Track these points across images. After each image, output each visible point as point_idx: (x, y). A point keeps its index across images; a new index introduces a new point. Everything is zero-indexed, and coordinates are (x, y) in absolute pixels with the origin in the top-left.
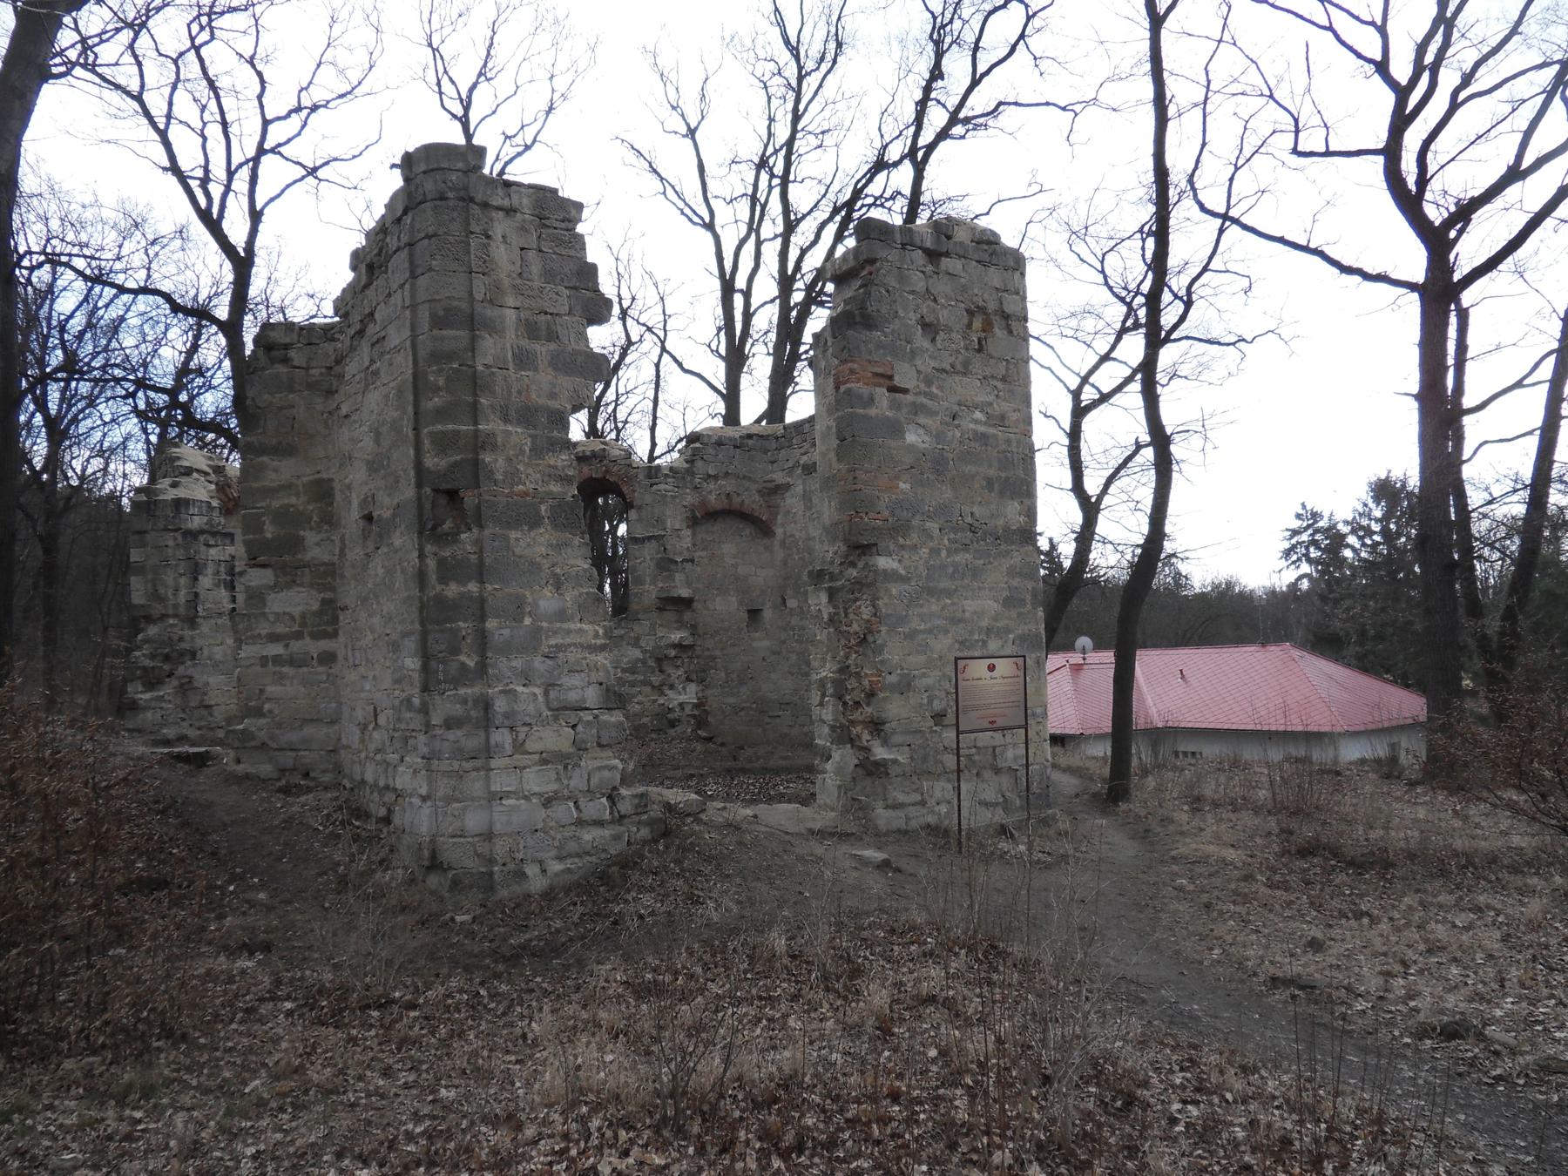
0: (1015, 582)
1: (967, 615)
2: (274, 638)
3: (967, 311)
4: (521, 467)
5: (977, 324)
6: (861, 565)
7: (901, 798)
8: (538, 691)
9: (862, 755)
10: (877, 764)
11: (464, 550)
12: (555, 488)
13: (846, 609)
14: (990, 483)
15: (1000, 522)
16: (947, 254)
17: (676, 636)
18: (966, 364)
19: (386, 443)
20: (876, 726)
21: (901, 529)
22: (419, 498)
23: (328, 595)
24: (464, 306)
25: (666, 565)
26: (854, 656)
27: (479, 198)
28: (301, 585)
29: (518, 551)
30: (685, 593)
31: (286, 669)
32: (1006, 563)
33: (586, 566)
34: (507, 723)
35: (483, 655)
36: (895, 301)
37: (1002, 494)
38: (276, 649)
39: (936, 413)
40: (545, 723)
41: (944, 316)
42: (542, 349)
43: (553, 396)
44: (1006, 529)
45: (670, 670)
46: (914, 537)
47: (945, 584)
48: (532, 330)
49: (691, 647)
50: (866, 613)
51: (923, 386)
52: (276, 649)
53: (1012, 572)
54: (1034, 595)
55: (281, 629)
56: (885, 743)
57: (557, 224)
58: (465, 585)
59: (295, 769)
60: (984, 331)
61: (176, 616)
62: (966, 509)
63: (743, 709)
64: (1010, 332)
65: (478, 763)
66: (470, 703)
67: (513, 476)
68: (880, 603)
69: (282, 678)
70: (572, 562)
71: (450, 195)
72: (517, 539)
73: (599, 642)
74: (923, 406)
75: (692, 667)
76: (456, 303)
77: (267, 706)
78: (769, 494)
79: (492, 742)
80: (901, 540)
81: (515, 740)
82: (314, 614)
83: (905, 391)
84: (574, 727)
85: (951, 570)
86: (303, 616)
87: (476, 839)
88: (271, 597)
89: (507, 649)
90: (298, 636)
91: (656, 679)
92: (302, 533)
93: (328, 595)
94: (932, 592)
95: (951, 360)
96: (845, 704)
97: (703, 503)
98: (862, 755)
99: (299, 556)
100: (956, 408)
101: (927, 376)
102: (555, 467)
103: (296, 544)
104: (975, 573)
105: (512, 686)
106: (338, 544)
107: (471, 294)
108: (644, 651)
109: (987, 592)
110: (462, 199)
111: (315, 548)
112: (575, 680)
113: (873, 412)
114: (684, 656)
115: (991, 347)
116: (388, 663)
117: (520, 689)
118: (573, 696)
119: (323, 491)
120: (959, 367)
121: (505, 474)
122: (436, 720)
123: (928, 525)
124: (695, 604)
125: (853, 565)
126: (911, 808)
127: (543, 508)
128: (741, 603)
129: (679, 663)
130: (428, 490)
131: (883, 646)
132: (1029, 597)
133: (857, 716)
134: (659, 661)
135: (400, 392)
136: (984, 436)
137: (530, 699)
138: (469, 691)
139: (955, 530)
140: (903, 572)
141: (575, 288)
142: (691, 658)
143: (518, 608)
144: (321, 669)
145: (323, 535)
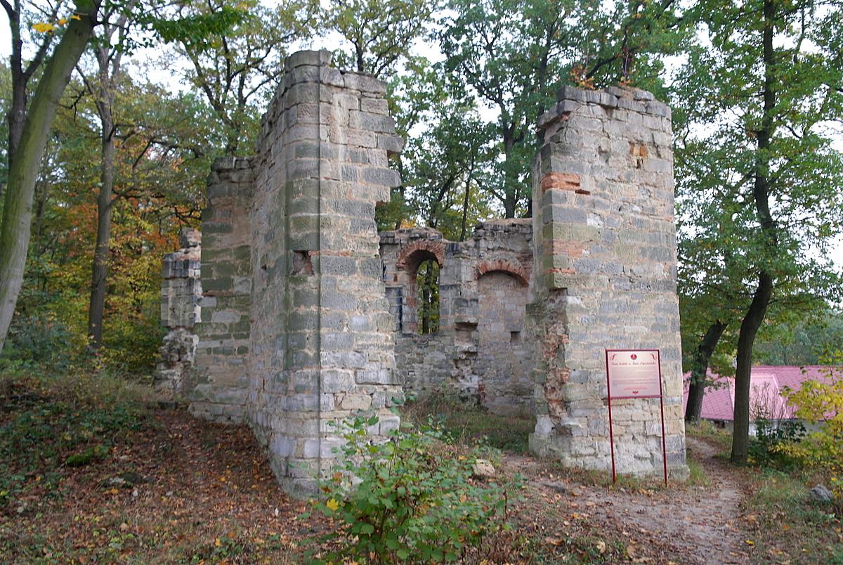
0: (661, 315)
1: (627, 335)
2: (215, 337)
3: (630, 143)
4: (345, 238)
5: (636, 151)
6: (557, 301)
7: (583, 451)
8: (350, 372)
9: (556, 422)
10: (564, 428)
11: (310, 286)
12: (365, 250)
13: (547, 329)
14: (644, 251)
15: (651, 276)
16: (617, 108)
17: (466, 346)
18: (629, 176)
19: (273, 224)
20: (565, 403)
21: (583, 279)
22: (287, 255)
23: (245, 313)
24: (315, 143)
25: (461, 302)
26: (552, 358)
27: (325, 81)
28: (231, 307)
29: (341, 288)
30: (472, 320)
31: (220, 356)
32: (654, 302)
33: (382, 298)
34: (331, 391)
35: (319, 350)
36: (581, 138)
37: (651, 257)
38: (216, 344)
39: (608, 207)
40: (353, 392)
41: (614, 146)
42: (360, 168)
43: (365, 196)
44: (655, 280)
45: (462, 367)
46: (591, 284)
47: (612, 315)
48: (354, 157)
49: (475, 353)
50: (560, 331)
51: (599, 190)
52: (216, 344)
53: (658, 308)
54: (673, 324)
55: (218, 332)
56: (570, 415)
57: (372, 95)
58: (309, 307)
59: (223, 415)
60: (641, 155)
61: (184, 327)
62: (627, 268)
63: (506, 393)
64: (659, 156)
65: (314, 414)
66: (310, 378)
67: (339, 242)
68: (568, 325)
69: (218, 361)
70: (375, 295)
71: (308, 79)
72: (341, 281)
73: (388, 344)
74: (598, 201)
75: (476, 366)
76: (310, 142)
77: (209, 377)
78: (525, 260)
79: (322, 402)
80: (583, 286)
81: (336, 401)
82: (237, 324)
83: (587, 193)
84: (372, 395)
85: (616, 306)
86: (231, 325)
87: (311, 460)
88: (214, 314)
89: (333, 346)
90: (228, 337)
91: (454, 372)
92: (232, 277)
93: (245, 313)
94: (602, 319)
95: (618, 174)
96: (546, 389)
97: (485, 265)
98: (556, 422)
99: (230, 290)
100: (621, 203)
101: (601, 184)
102: (365, 238)
103: (228, 283)
104: (632, 308)
105: (335, 369)
106: (251, 283)
107: (319, 137)
108: (447, 355)
109: (641, 320)
110: (316, 82)
111: (240, 286)
112: (374, 367)
113: (565, 206)
114: (471, 358)
115: (645, 165)
116: (270, 353)
117: (340, 370)
118: (372, 377)
119: (244, 252)
120: (623, 178)
121: (335, 242)
122: (291, 387)
123: (601, 277)
124: (478, 328)
125: (553, 301)
126: (587, 457)
127: (357, 262)
128: (507, 327)
129: (468, 362)
130: (291, 251)
131: (570, 352)
132: (669, 325)
133: (553, 396)
134: (456, 361)
135: (280, 197)
136: (641, 221)
137: (345, 377)
138: (309, 370)
139: (620, 280)
140: (584, 307)
141: (381, 133)
142: (475, 360)
143: (340, 322)
144: (240, 356)
145: (244, 278)
